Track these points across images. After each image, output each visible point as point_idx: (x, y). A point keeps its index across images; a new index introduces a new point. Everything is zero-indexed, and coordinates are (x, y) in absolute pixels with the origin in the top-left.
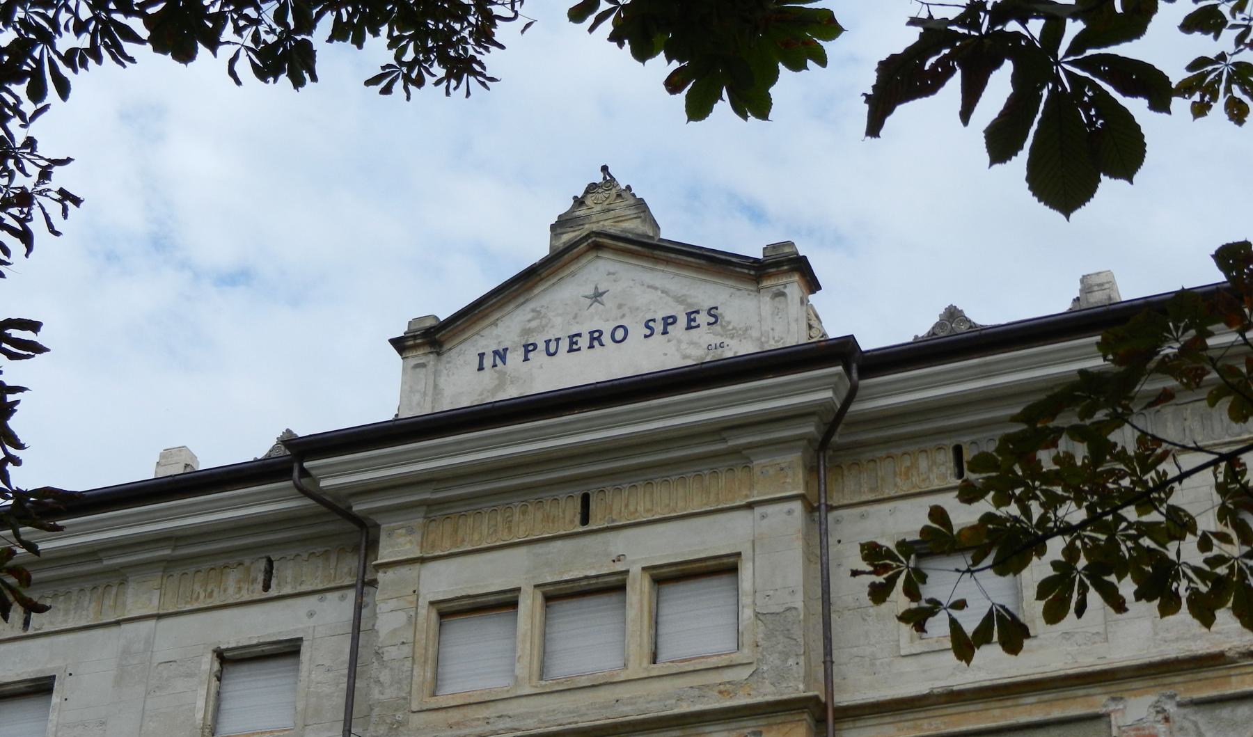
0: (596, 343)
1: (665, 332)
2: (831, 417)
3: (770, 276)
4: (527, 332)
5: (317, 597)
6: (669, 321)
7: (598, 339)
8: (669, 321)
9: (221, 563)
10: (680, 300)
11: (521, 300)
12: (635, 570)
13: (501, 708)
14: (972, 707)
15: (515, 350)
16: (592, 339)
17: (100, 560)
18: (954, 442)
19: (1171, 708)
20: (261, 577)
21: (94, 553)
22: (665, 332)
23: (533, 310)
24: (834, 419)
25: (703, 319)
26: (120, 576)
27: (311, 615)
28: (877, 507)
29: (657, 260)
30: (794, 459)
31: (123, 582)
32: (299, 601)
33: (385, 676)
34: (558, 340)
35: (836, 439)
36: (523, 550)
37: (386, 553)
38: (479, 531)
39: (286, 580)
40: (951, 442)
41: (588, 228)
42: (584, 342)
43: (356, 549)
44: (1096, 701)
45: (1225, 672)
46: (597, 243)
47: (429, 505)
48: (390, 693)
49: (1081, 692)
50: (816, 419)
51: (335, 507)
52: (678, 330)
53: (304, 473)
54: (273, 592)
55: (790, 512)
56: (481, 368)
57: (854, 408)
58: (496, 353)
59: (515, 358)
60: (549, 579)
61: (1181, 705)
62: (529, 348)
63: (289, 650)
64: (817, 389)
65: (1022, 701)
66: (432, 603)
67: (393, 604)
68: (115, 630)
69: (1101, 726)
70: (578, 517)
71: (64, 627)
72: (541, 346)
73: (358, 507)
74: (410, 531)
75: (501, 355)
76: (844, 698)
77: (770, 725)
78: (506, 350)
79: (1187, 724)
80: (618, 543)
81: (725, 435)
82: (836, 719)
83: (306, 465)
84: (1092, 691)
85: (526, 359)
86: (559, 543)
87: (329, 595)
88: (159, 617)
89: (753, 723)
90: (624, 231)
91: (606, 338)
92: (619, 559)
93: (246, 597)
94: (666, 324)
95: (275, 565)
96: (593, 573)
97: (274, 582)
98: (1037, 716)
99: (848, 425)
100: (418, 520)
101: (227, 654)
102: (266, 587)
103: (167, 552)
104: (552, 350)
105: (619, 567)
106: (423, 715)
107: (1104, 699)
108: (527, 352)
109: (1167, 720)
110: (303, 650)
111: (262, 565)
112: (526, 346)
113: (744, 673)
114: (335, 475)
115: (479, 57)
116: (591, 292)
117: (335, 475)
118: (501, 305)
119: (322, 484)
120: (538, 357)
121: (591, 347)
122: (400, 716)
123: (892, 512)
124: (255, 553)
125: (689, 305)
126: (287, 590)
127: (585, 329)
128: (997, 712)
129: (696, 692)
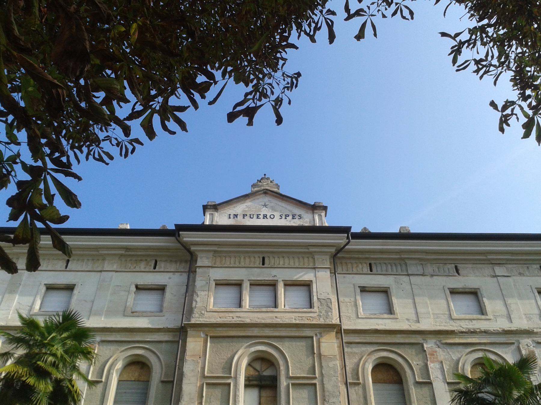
2: (339, 249)
3: (317, 210)
4: (244, 211)
5: (172, 273)
7: (266, 217)
8: (287, 216)
9: (139, 259)
12: (280, 280)
14: (382, 335)
18: (369, 262)
20: (153, 265)
22: (286, 218)
24: (340, 250)
26: (103, 258)
27: (170, 278)
28: (348, 275)
29: (283, 200)
30: (328, 257)
31: (104, 260)
32: (165, 274)
33: (198, 299)
35: (339, 255)
37: (199, 263)
39: (161, 266)
40: (368, 262)
41: (262, 188)
42: (261, 217)
43: (186, 262)
46: (266, 192)
47: (215, 251)
49: (413, 336)
51: (186, 247)
54: (156, 270)
57: (347, 247)
58: (234, 215)
60: (253, 279)
61: (442, 344)
62: (244, 216)
63: (161, 289)
64: (340, 239)
66: (214, 280)
67: (201, 278)
70: (261, 263)
71: (80, 270)
72: (248, 216)
73: (193, 248)
74: (208, 258)
76: (344, 327)
77: (324, 331)
80: (274, 272)
81: (309, 247)
83: (180, 233)
84: (417, 336)
86: (256, 269)
87: (176, 273)
88: (117, 272)
89: (319, 330)
91: (268, 217)
92: (275, 276)
95: (158, 262)
96: (267, 279)
97: (157, 267)
98: (402, 341)
99: (344, 252)
100: (211, 255)
101: (139, 286)
103: (123, 252)
105: (275, 278)
106: (210, 313)
107: (421, 339)
111: (154, 262)
114: (188, 237)
116: (263, 204)
118: (237, 202)
119: (184, 239)
122: (203, 312)
123: (353, 277)
124: (154, 260)
126: (162, 270)
128: (389, 338)
129: (300, 318)
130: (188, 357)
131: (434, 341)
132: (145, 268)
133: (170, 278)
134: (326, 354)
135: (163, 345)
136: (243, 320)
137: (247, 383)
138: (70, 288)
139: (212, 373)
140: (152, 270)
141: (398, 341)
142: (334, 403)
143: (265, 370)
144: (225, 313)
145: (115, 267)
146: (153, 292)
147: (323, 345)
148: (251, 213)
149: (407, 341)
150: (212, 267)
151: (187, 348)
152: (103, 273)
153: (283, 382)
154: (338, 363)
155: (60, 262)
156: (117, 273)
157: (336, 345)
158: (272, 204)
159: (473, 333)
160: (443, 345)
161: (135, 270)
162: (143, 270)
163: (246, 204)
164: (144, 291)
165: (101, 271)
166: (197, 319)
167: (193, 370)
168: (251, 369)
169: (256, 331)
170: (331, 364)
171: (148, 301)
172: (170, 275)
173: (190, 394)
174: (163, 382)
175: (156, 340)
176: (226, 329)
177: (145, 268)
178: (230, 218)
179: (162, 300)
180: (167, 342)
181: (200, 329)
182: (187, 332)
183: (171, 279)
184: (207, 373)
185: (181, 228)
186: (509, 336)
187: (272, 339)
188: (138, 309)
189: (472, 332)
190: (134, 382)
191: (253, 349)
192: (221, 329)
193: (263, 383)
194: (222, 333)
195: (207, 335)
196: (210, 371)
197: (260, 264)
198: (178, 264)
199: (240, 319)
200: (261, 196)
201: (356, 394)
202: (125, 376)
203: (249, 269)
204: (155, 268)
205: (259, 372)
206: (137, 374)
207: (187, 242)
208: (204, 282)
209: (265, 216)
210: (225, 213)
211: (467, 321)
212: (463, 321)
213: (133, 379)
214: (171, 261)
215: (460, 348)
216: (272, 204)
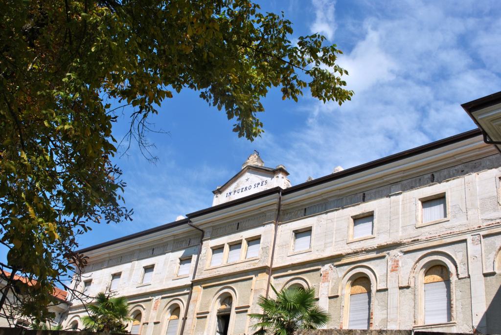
4: (235, 188)
6: (259, 184)
8: (259, 184)
10: (261, 179)
13: (218, 269)
17: (383, 179)
19: (333, 267)
21: (381, 177)
25: (264, 183)
50: (276, 205)
52: (259, 186)
53: (190, 222)
59: (232, 194)
61: (334, 266)
62: (235, 191)
64: (274, 199)
69: (251, 281)
73: (201, 228)
75: (230, 193)
82: (272, 271)
90: (254, 165)
102: (189, 245)
110: (374, 214)
113: (258, 260)
114: (196, 221)
115: (60, 201)
120: (236, 193)
159: (356, 253)
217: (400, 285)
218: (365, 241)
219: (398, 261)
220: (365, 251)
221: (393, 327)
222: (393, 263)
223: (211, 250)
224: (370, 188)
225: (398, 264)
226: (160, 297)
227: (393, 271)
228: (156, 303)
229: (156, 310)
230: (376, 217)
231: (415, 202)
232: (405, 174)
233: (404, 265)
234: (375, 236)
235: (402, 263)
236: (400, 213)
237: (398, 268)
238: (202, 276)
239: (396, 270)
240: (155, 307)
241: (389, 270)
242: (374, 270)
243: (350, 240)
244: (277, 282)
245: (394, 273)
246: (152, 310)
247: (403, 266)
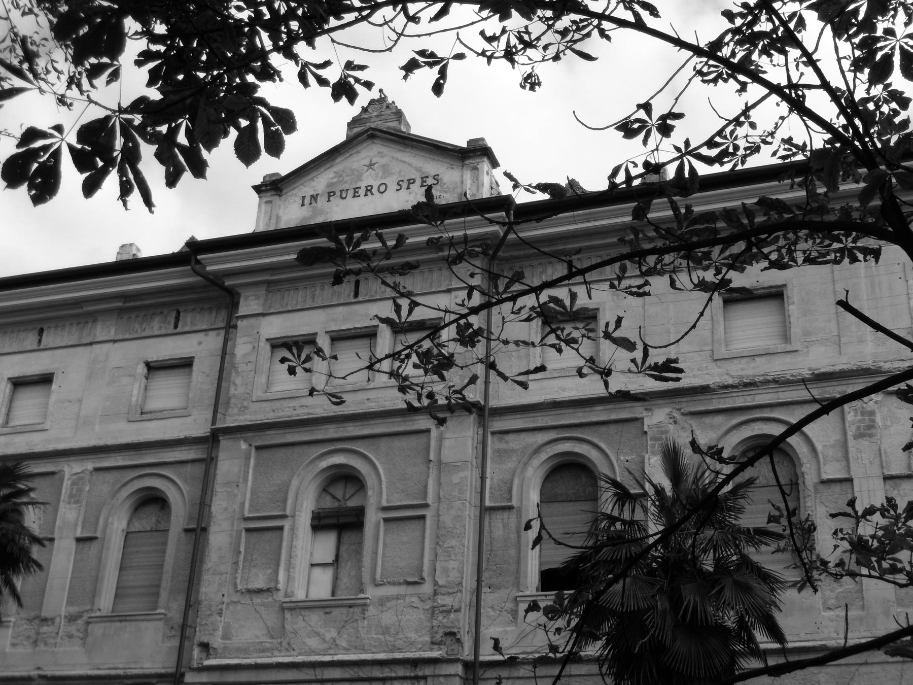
0: (369, 193)
1: (408, 188)
3: (469, 158)
4: (329, 185)
5: (203, 333)
7: (370, 190)
8: (411, 182)
10: (418, 170)
11: (328, 165)
15: (322, 195)
16: (367, 190)
19: (677, 415)
20: (173, 321)
22: (408, 188)
23: (335, 172)
26: (93, 317)
27: (200, 343)
29: (406, 146)
31: (95, 321)
33: (238, 381)
34: (347, 190)
36: (320, 311)
38: (297, 298)
42: (362, 192)
44: (637, 410)
45: (709, 397)
46: (373, 135)
47: (269, 283)
48: (240, 390)
51: (215, 281)
55: (243, 409)
56: (303, 205)
60: (334, 328)
61: (683, 414)
62: (330, 194)
63: (186, 364)
65: (595, 408)
66: (267, 340)
67: (245, 339)
68: (89, 348)
72: (338, 194)
73: (228, 283)
74: (257, 298)
75: (314, 198)
76: (493, 403)
78: (317, 195)
79: (686, 425)
83: (199, 257)
85: (329, 201)
86: (341, 308)
87: (210, 333)
88: (114, 341)
91: (375, 190)
93: (163, 332)
94: (409, 183)
98: (603, 417)
100: (262, 291)
104: (344, 196)
106: (259, 404)
108: (330, 196)
109: (675, 422)
111: (174, 314)
112: (329, 193)
116: (367, 162)
117: (215, 264)
119: (208, 268)
121: (366, 195)
122: (245, 404)
125: (423, 173)
126: (187, 329)
127: (363, 185)
128: (580, 414)
130: (218, 488)
131: (667, 410)
132: (161, 327)
133: (200, 343)
134: (449, 461)
135: (189, 468)
136: (311, 411)
137: (316, 523)
138: (45, 380)
139: (257, 511)
140: (171, 330)
141: (595, 419)
142: (452, 547)
143: (353, 495)
144: (282, 402)
145: (112, 334)
146: (177, 371)
147: (446, 443)
148: (344, 187)
149: (614, 416)
150: (263, 315)
151: (218, 472)
152: (95, 346)
153: (372, 518)
154: (470, 476)
155: (30, 335)
156: (117, 345)
157: (470, 442)
158: (384, 161)
159: (749, 385)
160: (684, 418)
161: (144, 334)
162: (157, 333)
163: (335, 169)
164: (162, 373)
165: (91, 344)
166: (236, 417)
167: (226, 509)
168: (328, 498)
169: (331, 430)
170: (456, 479)
171: (167, 392)
172: (201, 336)
173: (219, 549)
174: (187, 531)
175: (176, 459)
176: (281, 431)
177: (161, 327)
178: (303, 205)
179: (190, 382)
180: (193, 461)
181: (238, 436)
182: (219, 441)
183: (200, 345)
184: (250, 511)
185: (195, 248)
186: (826, 384)
187: (360, 442)
188: (152, 405)
189: (746, 385)
190: (149, 534)
191: (324, 464)
192: (273, 432)
193: (342, 520)
194: (273, 437)
195: (250, 445)
196: (252, 508)
197: (349, 296)
198: (214, 315)
199: (306, 411)
200: (365, 144)
201: (504, 526)
202: (136, 524)
203: (329, 311)
204: (176, 327)
205: (339, 501)
206: (154, 519)
207: (216, 273)
208: (250, 347)
209: (369, 190)
210: (295, 195)
211: (744, 361)
212: (736, 361)
213: (148, 529)
214: (202, 309)
215: (719, 419)
216: (384, 161)
217: (887, 473)
218: (769, 357)
219: (872, 413)
220: (775, 381)
221: (477, 7)
222: (859, 417)
223: (268, 347)
224: (424, 248)
225: (874, 421)
226: (90, 466)
227: (859, 436)
228: (73, 484)
229: (77, 502)
230: (796, 299)
231: (902, 275)
232: (127, 305)
233: (889, 423)
234: (799, 348)
235: (884, 419)
236: (865, 298)
237: (873, 431)
238: (248, 417)
239: (871, 436)
240: (71, 496)
241: (850, 433)
242: (814, 440)
243: (722, 352)
244: (503, 446)
245: (864, 443)
246: (61, 504)
247: (886, 427)
